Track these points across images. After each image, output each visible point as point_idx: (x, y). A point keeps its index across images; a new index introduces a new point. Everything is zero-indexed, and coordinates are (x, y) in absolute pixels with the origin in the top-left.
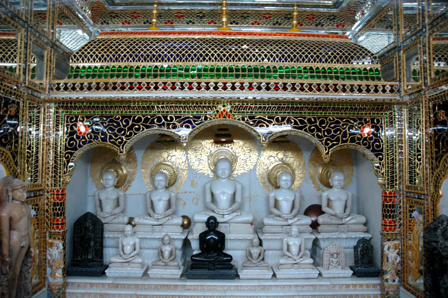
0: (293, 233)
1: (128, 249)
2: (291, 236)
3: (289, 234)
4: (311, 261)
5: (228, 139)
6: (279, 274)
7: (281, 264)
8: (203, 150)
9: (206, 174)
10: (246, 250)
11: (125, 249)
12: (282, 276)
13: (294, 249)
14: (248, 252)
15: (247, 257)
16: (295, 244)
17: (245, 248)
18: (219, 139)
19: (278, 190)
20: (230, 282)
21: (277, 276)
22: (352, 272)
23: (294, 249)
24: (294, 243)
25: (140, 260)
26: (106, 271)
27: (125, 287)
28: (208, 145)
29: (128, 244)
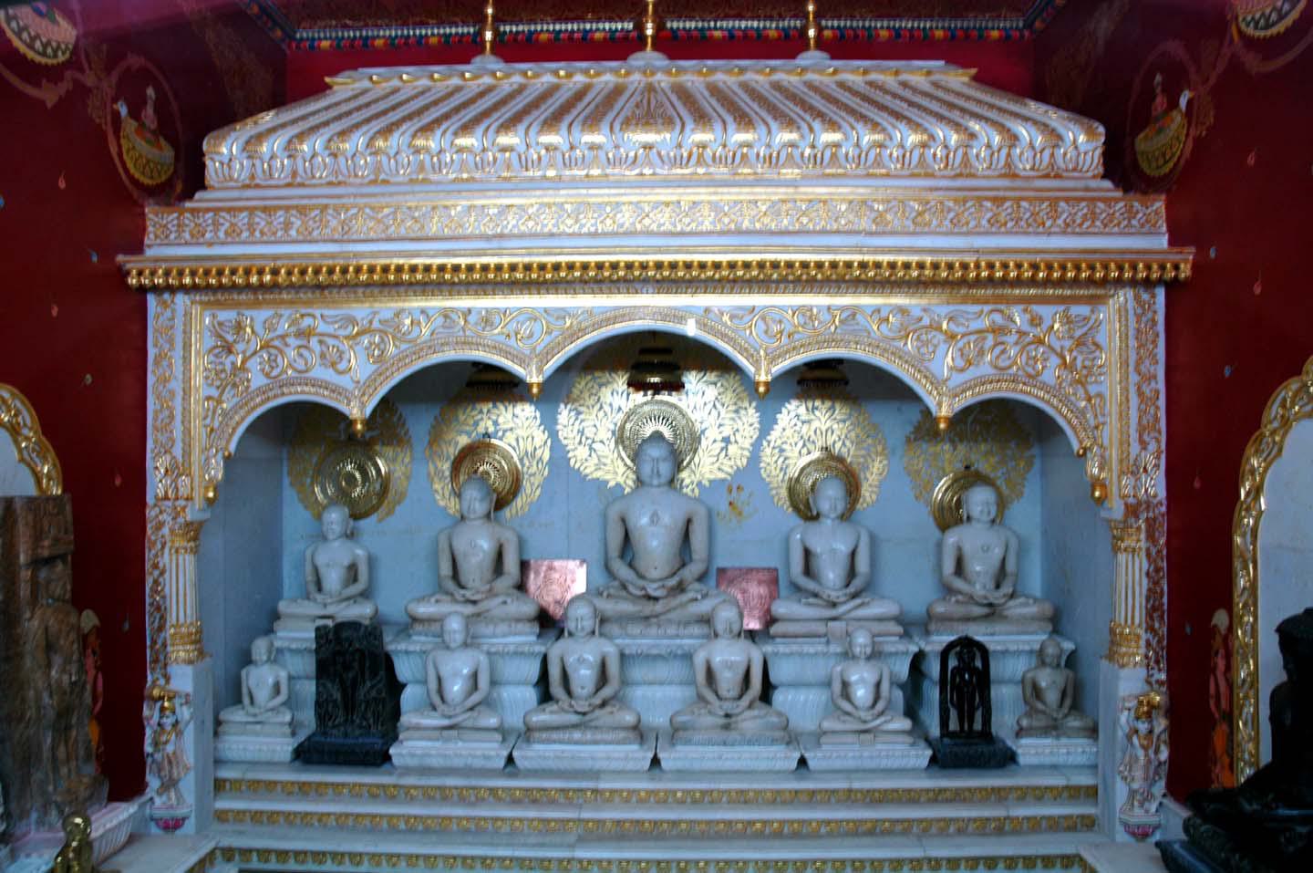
0: (857, 650)
1: (456, 688)
2: (854, 657)
3: (848, 655)
4: (906, 724)
5: (668, 377)
6: (524, 757)
7: (825, 733)
8: (601, 414)
9: (612, 484)
10: (1023, 681)
11: (446, 685)
12: (824, 765)
13: (862, 694)
14: (1029, 690)
15: (1026, 702)
16: (862, 680)
17: (1019, 675)
18: (639, 377)
19: (812, 526)
20: (361, 773)
21: (663, 764)
22: (929, 753)
23: (862, 694)
24: (862, 681)
25: (493, 721)
26: (392, 751)
27: (240, 789)
28: (616, 398)
29: (456, 674)
